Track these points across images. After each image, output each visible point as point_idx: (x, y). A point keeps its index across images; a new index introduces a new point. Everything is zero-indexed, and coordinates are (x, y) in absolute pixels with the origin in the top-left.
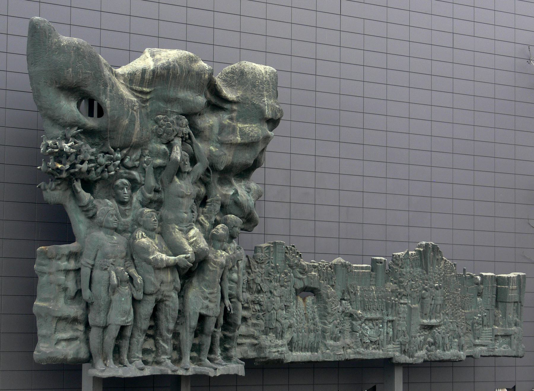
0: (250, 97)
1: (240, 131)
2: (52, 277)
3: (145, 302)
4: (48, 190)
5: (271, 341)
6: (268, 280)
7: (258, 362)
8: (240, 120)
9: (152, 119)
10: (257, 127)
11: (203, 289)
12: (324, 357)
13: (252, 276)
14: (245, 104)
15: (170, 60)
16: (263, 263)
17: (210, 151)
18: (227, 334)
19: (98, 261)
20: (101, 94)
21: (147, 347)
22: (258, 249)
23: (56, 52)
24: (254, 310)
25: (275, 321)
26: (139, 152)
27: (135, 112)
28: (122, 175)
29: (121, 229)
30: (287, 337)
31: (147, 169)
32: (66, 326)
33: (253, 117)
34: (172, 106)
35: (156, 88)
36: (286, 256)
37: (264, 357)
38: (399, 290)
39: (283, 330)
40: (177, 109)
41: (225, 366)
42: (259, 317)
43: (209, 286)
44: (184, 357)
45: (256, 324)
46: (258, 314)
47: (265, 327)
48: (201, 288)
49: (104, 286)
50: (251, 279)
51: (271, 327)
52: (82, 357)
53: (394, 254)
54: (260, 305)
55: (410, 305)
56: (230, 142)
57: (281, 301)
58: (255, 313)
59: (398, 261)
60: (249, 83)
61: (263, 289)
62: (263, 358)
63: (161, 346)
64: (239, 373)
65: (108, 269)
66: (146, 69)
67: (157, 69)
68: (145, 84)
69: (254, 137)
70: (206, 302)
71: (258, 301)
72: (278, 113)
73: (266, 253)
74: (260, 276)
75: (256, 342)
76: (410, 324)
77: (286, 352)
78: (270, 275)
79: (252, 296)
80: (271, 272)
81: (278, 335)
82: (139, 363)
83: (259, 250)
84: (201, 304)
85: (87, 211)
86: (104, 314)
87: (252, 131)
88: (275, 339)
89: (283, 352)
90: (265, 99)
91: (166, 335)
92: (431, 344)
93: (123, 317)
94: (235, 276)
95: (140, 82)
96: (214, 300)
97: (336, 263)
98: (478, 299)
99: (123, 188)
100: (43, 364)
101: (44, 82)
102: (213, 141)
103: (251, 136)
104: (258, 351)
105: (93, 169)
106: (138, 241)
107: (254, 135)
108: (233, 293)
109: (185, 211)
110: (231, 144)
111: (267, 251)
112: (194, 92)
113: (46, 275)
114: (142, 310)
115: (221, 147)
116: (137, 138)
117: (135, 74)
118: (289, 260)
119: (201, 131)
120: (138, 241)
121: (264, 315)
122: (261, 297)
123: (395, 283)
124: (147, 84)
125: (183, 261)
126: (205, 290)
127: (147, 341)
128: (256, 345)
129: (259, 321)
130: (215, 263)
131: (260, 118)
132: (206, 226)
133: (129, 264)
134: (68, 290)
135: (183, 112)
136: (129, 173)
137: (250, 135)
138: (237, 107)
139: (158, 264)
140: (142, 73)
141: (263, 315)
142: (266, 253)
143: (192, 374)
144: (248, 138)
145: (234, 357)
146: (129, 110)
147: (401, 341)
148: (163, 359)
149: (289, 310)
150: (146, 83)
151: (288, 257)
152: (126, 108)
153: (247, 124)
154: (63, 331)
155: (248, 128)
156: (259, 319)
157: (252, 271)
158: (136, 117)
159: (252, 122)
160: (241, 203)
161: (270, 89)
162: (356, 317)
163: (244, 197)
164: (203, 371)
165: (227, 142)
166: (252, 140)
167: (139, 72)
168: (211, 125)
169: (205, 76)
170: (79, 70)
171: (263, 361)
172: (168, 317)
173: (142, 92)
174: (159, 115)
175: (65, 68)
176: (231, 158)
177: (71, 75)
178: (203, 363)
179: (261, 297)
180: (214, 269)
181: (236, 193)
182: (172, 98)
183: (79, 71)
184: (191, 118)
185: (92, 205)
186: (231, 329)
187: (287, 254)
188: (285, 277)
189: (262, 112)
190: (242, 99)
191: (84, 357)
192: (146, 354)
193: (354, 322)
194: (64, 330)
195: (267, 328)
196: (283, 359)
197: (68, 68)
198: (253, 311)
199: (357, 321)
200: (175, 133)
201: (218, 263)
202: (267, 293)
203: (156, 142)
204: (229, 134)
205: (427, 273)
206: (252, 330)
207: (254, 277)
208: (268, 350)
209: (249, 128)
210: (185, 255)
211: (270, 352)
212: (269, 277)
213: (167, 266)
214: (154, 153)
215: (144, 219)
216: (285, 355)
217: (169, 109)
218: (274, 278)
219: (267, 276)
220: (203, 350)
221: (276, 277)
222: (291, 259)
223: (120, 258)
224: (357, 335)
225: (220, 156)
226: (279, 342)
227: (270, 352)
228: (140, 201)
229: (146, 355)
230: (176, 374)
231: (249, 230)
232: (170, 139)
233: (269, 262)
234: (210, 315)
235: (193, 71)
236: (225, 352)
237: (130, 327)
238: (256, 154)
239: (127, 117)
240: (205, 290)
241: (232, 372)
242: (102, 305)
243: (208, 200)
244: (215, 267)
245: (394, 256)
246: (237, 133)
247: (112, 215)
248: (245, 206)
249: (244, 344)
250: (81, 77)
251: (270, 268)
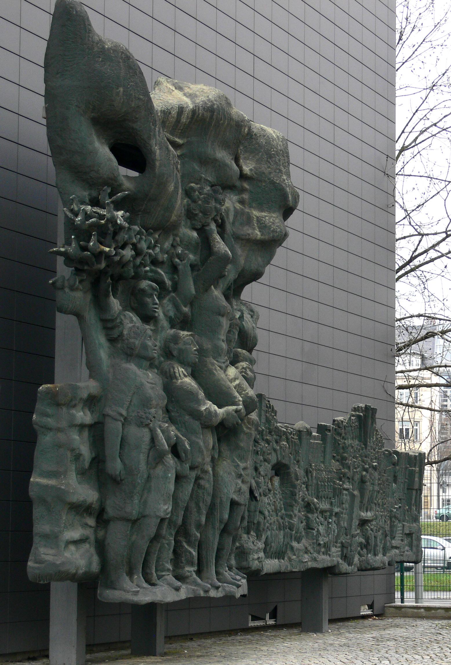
0: (267, 171)
2: (61, 437)
3: (185, 480)
4: (67, 290)
11: (237, 463)
12: (292, 565)
14: (260, 181)
15: (210, 97)
19: (133, 411)
23: (100, 57)
31: (180, 267)
35: (189, 139)
37: (247, 566)
38: (343, 470)
44: (207, 568)
49: (144, 453)
53: (336, 419)
55: (351, 490)
59: (341, 430)
60: (262, 150)
63: (187, 550)
65: (151, 425)
66: (183, 108)
67: (199, 109)
69: (276, 232)
76: (351, 519)
78: (256, 444)
85: (112, 328)
91: (195, 534)
92: (363, 546)
97: (301, 429)
98: (393, 484)
99: (151, 295)
100: (42, 582)
101: (76, 106)
106: (180, 381)
113: (51, 433)
114: (181, 494)
117: (170, 113)
120: (181, 382)
123: (338, 461)
124: (180, 131)
134: (81, 458)
136: (156, 272)
137: (272, 229)
139: (211, 420)
140: (178, 112)
147: (344, 541)
148: (188, 571)
150: (179, 130)
155: (267, 218)
162: (314, 507)
165: (243, 237)
166: (273, 236)
167: (176, 111)
170: (131, 92)
172: (201, 504)
175: (114, 86)
177: (121, 99)
183: (132, 94)
190: (255, 173)
193: (310, 515)
195: (250, 524)
197: (118, 87)
199: (313, 513)
201: (253, 421)
204: (242, 224)
205: (366, 448)
209: (270, 219)
210: (234, 407)
215: (181, 346)
224: (313, 533)
228: (170, 318)
242: (139, 483)
244: (249, 428)
245: (336, 422)
246: (254, 225)
248: (250, 337)
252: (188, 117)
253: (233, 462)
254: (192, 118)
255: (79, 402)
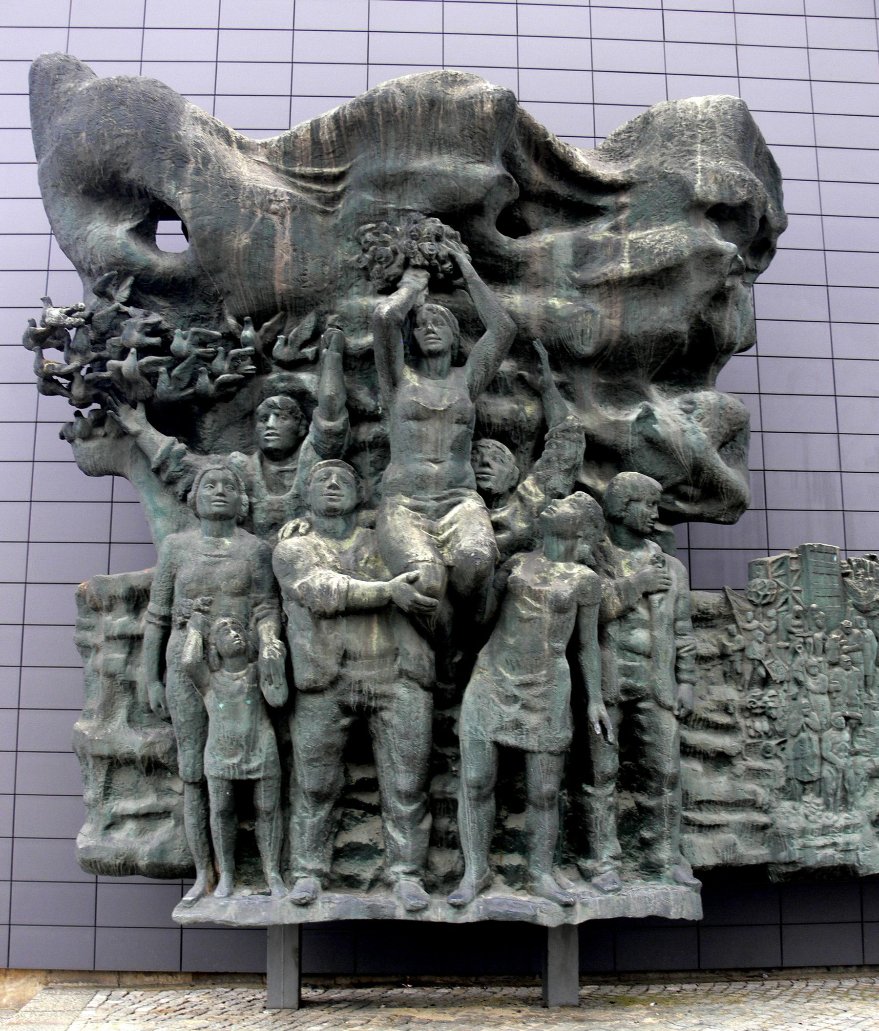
1: (631, 247)
5: (806, 817)
6: (787, 648)
7: (779, 875)
8: (638, 224)
9: (350, 236)
10: (675, 229)
11: (501, 674)
13: (739, 642)
14: (645, 182)
16: (768, 604)
17: (549, 309)
18: (644, 799)
20: (165, 180)
21: (360, 840)
22: (755, 567)
24: (752, 733)
25: (817, 761)
26: (308, 322)
27: (275, 218)
28: (274, 388)
29: (262, 521)
30: (867, 804)
32: (138, 782)
33: (666, 207)
34: (399, 197)
35: (354, 161)
36: (844, 584)
39: (847, 786)
40: (414, 202)
41: (610, 895)
42: (768, 753)
43: (519, 665)
45: (763, 770)
46: (765, 742)
47: (789, 780)
48: (496, 669)
50: (735, 648)
51: (806, 778)
52: (176, 862)
54: (771, 719)
56: (602, 280)
57: (833, 705)
58: (755, 741)
61: (772, 674)
62: (786, 864)
64: (669, 912)
68: (326, 157)
69: (665, 253)
70: (513, 710)
71: (762, 707)
72: (738, 189)
73: (778, 576)
74: (761, 639)
75: (763, 819)
77: (861, 846)
78: (791, 636)
79: (743, 694)
80: (794, 626)
81: (831, 799)
82: (306, 884)
83: (759, 570)
84: (496, 718)
86: (193, 749)
87: (659, 241)
88: (823, 811)
89: (851, 847)
90: (699, 158)
93: (233, 755)
94: (640, 636)
95: (312, 154)
96: (539, 703)
102: (559, 286)
103: (658, 254)
104: (772, 844)
105: (162, 369)
107: (664, 248)
108: (639, 685)
109: (432, 456)
110: (607, 283)
111: (781, 572)
112: (461, 155)
115: (583, 297)
116: (286, 281)
118: (855, 593)
119: (518, 264)
121: (783, 746)
122: (769, 697)
125: (401, 590)
126: (508, 675)
127: (363, 822)
128: (765, 827)
129: (770, 761)
130: (536, 596)
131: (683, 205)
132: (531, 501)
133: (264, 612)
135: (434, 209)
137: (656, 251)
138: (630, 197)
140: (312, 129)
141: (779, 744)
142: (778, 576)
143: (475, 920)
144: (650, 259)
145: (667, 866)
146: (253, 214)
149: (868, 729)
150: (328, 154)
151: (852, 586)
152: (244, 207)
153: (650, 229)
154: (132, 795)
156: (770, 758)
157: (738, 627)
158: (279, 227)
159: (663, 220)
160: (664, 441)
161: (716, 137)
163: (673, 425)
164: (514, 910)
165: (596, 282)
168: (548, 244)
169: (482, 107)
170: (101, 131)
171: (788, 873)
172: (394, 755)
173: (318, 178)
174: (365, 223)
176: (616, 322)
178: (536, 884)
179: (769, 697)
180: (535, 614)
181: (648, 416)
182: (392, 175)
184: (472, 226)
185: (178, 464)
186: (651, 787)
187: (851, 578)
188: (842, 638)
189: (685, 188)
191: (183, 863)
192: (357, 858)
194: (135, 792)
196: (854, 866)
198: (751, 737)
200: (401, 257)
201: (545, 597)
202: (785, 686)
203: (363, 294)
206: (749, 788)
207: (743, 644)
208: (798, 843)
210: (404, 576)
211: (804, 847)
212: (789, 640)
213: (346, 608)
214: (357, 320)
216: (861, 853)
217: (391, 206)
218: (804, 643)
219: (785, 638)
220: (534, 849)
221: (810, 640)
222: (861, 591)
223: (225, 593)
225: (575, 316)
226: (835, 818)
227: (804, 847)
229: (358, 862)
230: (419, 919)
231: (722, 519)
232: (389, 276)
233: (786, 602)
234: (530, 748)
235: (451, 101)
236: (643, 850)
237: (262, 783)
238: (687, 304)
239: (246, 230)
240: (508, 675)
241: (637, 911)
243: (546, 436)
244: (537, 609)
246: (623, 256)
247: (214, 482)
248: (678, 447)
249: (723, 825)
250: (107, 147)
251: (790, 616)
252: (329, 128)
253: (495, 675)
254: (338, 128)
255: (610, 575)
